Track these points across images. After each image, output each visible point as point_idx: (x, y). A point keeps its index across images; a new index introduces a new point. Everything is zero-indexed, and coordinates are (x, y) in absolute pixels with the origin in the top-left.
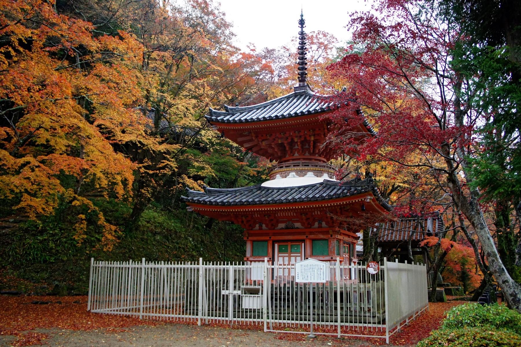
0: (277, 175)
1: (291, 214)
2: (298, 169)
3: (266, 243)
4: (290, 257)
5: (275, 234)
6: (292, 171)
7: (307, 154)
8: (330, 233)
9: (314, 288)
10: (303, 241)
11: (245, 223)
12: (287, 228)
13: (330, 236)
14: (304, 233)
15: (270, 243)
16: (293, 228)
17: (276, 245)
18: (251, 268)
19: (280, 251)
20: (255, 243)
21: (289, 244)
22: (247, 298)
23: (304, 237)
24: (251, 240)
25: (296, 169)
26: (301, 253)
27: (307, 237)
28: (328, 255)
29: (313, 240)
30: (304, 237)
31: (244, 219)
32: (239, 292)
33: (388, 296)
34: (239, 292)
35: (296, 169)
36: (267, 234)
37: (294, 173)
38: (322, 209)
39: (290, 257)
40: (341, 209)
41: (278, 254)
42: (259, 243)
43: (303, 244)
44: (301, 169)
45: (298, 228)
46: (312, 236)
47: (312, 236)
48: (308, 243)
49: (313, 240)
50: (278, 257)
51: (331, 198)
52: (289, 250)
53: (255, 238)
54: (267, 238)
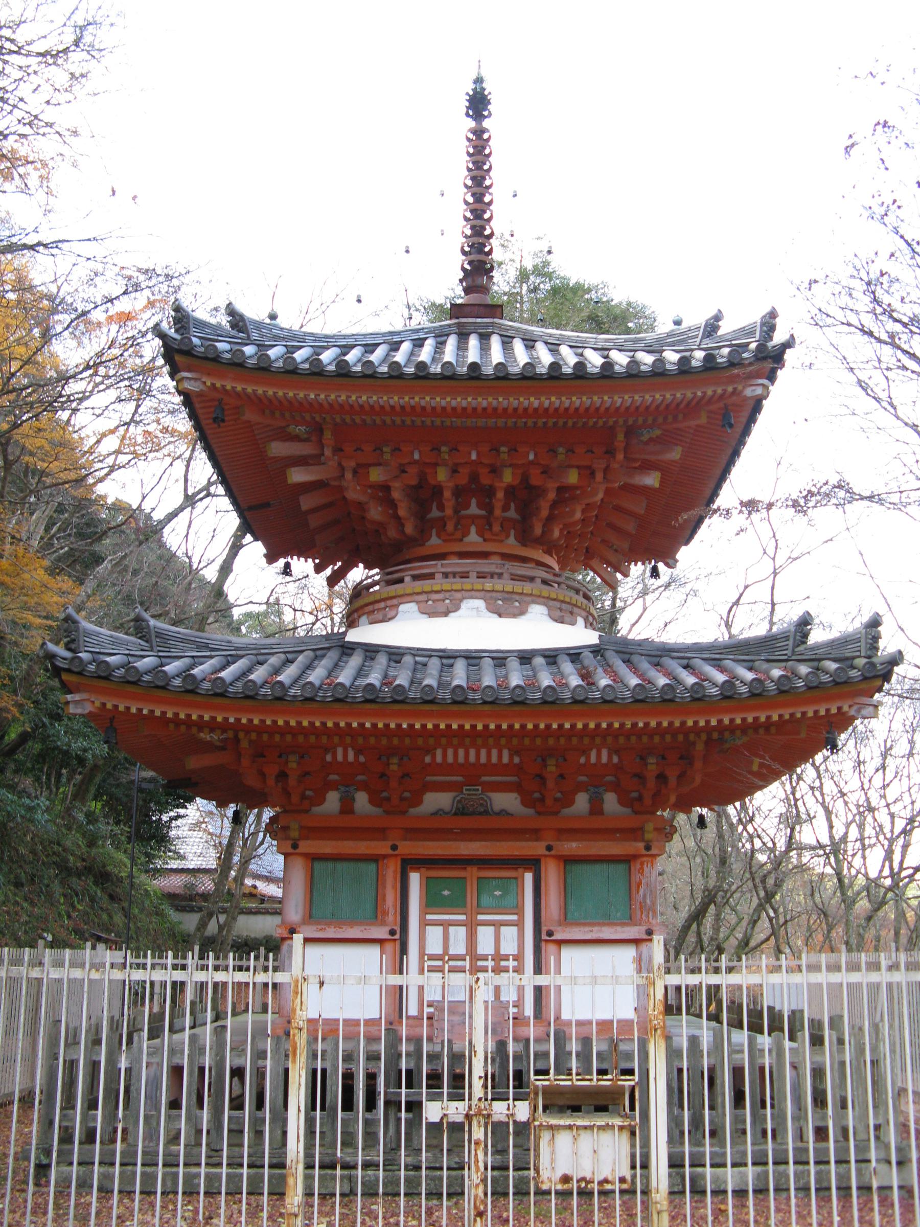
0: (402, 608)
1: (456, 755)
2: (499, 587)
3: (372, 867)
4: (472, 928)
5: (416, 832)
6: (472, 593)
7: (512, 540)
8: (648, 836)
9: (372, 1039)
10: (533, 864)
11: (292, 781)
12: (461, 811)
13: (641, 845)
14: (535, 834)
15: (391, 871)
16: (486, 812)
17: (415, 879)
18: (558, 989)
19: (431, 902)
20: (318, 866)
21: (473, 873)
22: (564, 1140)
23: (537, 848)
24: (306, 855)
25: (488, 586)
26: (519, 910)
27: (549, 848)
28: (631, 920)
29: (568, 861)
30: (537, 848)
31: (293, 765)
32: (522, 1111)
33: (867, 1101)
34: (522, 1111)
35: (488, 586)
36: (379, 833)
37: (480, 604)
38: (622, 740)
39: (472, 928)
40: (709, 742)
41: (423, 911)
42: (339, 866)
43: (529, 877)
44: (509, 588)
45: (503, 813)
46: (572, 847)
47: (572, 847)
48: (552, 874)
49: (568, 861)
50: (424, 924)
51: (757, 694)
52: (471, 897)
53: (327, 847)
54: (381, 847)
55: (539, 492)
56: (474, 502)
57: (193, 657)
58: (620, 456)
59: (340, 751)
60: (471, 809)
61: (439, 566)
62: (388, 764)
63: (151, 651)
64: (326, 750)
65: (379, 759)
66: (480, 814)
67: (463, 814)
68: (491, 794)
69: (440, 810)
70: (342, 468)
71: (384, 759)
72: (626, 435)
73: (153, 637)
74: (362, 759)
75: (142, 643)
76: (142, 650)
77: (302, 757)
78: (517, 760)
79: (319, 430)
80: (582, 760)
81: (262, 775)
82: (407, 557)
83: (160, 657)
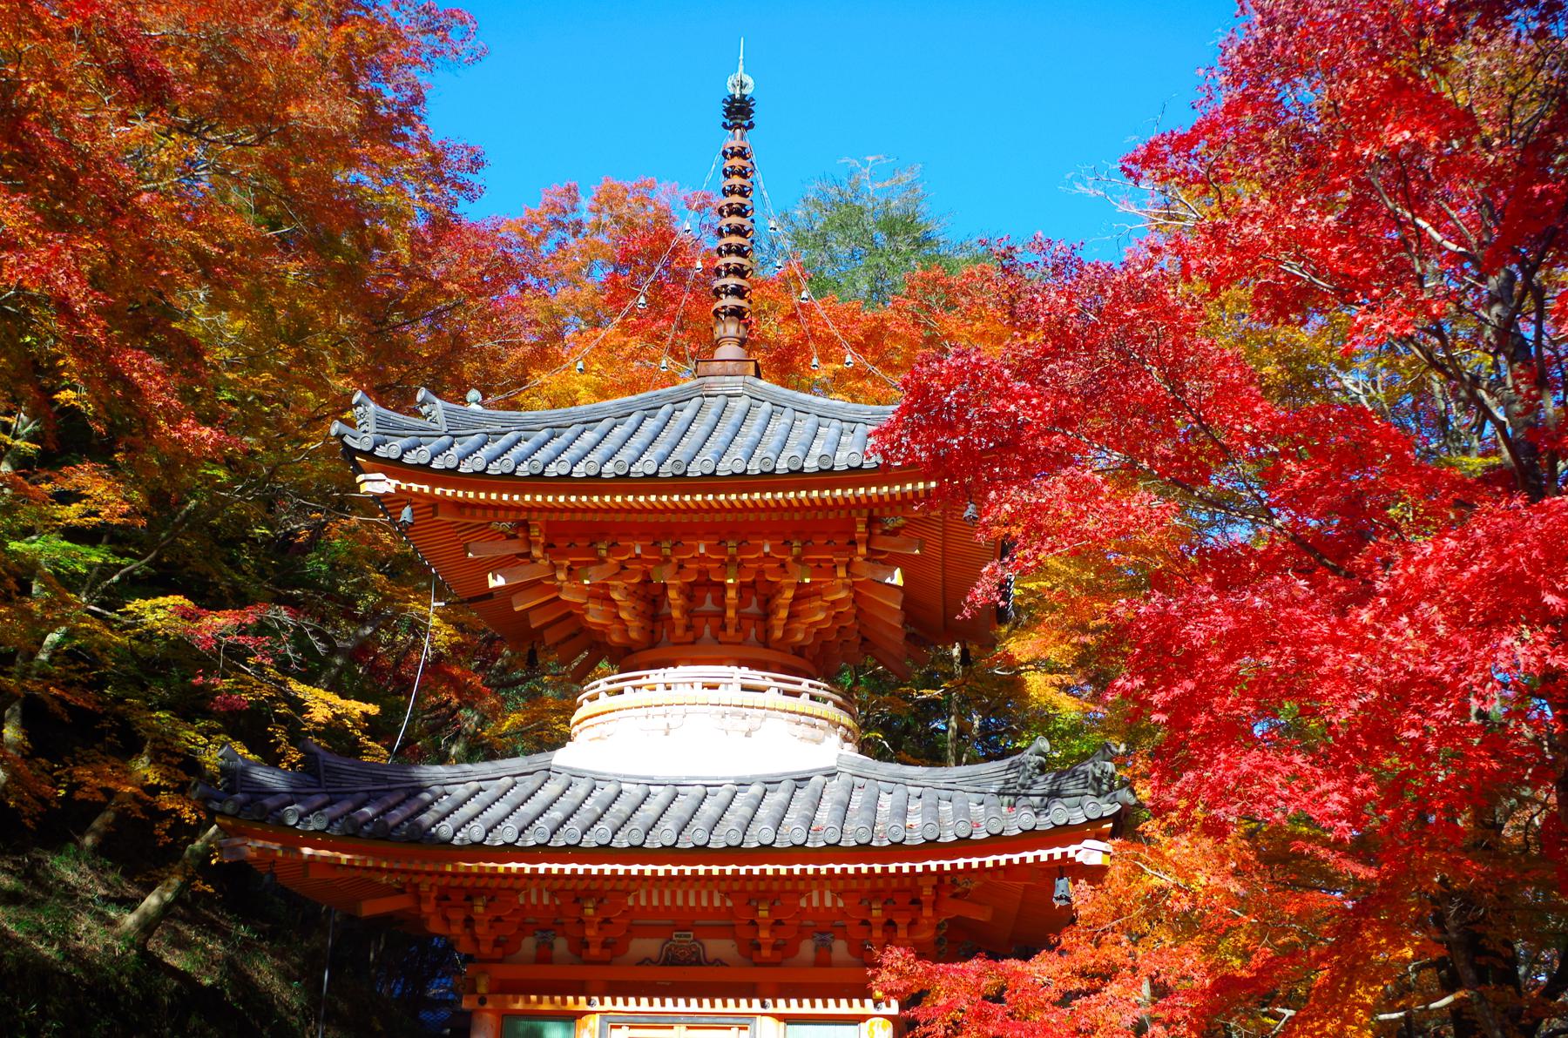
45: (718, 962)
55: (777, 590)
56: (709, 596)
57: (368, 791)
58: (862, 550)
59: (815, 895)
60: (682, 958)
61: (661, 675)
62: (757, 910)
63: (320, 787)
64: (802, 894)
65: (748, 903)
66: (692, 964)
67: (672, 964)
68: (705, 941)
69: (647, 959)
70: (554, 567)
71: (754, 904)
72: (867, 526)
73: (322, 770)
74: (729, 903)
75: (309, 779)
76: (309, 787)
77: (773, 904)
78: (729, 903)
79: (525, 525)
80: (803, 903)
81: (447, 921)
82: (635, 661)
83: (329, 793)
